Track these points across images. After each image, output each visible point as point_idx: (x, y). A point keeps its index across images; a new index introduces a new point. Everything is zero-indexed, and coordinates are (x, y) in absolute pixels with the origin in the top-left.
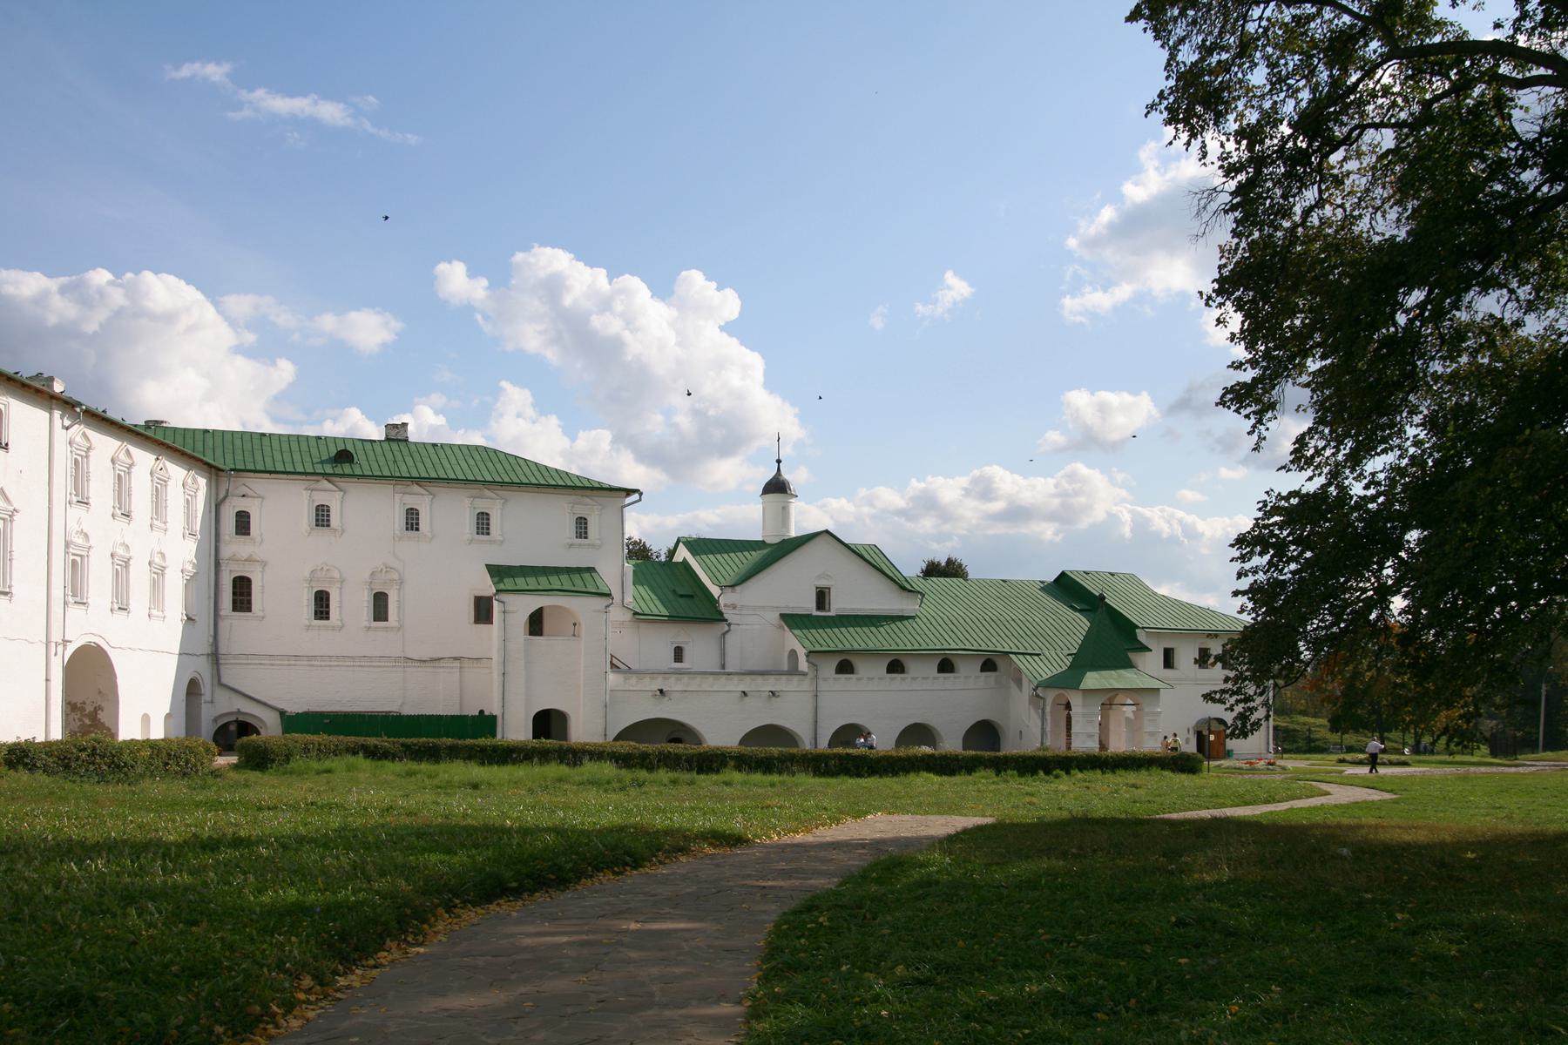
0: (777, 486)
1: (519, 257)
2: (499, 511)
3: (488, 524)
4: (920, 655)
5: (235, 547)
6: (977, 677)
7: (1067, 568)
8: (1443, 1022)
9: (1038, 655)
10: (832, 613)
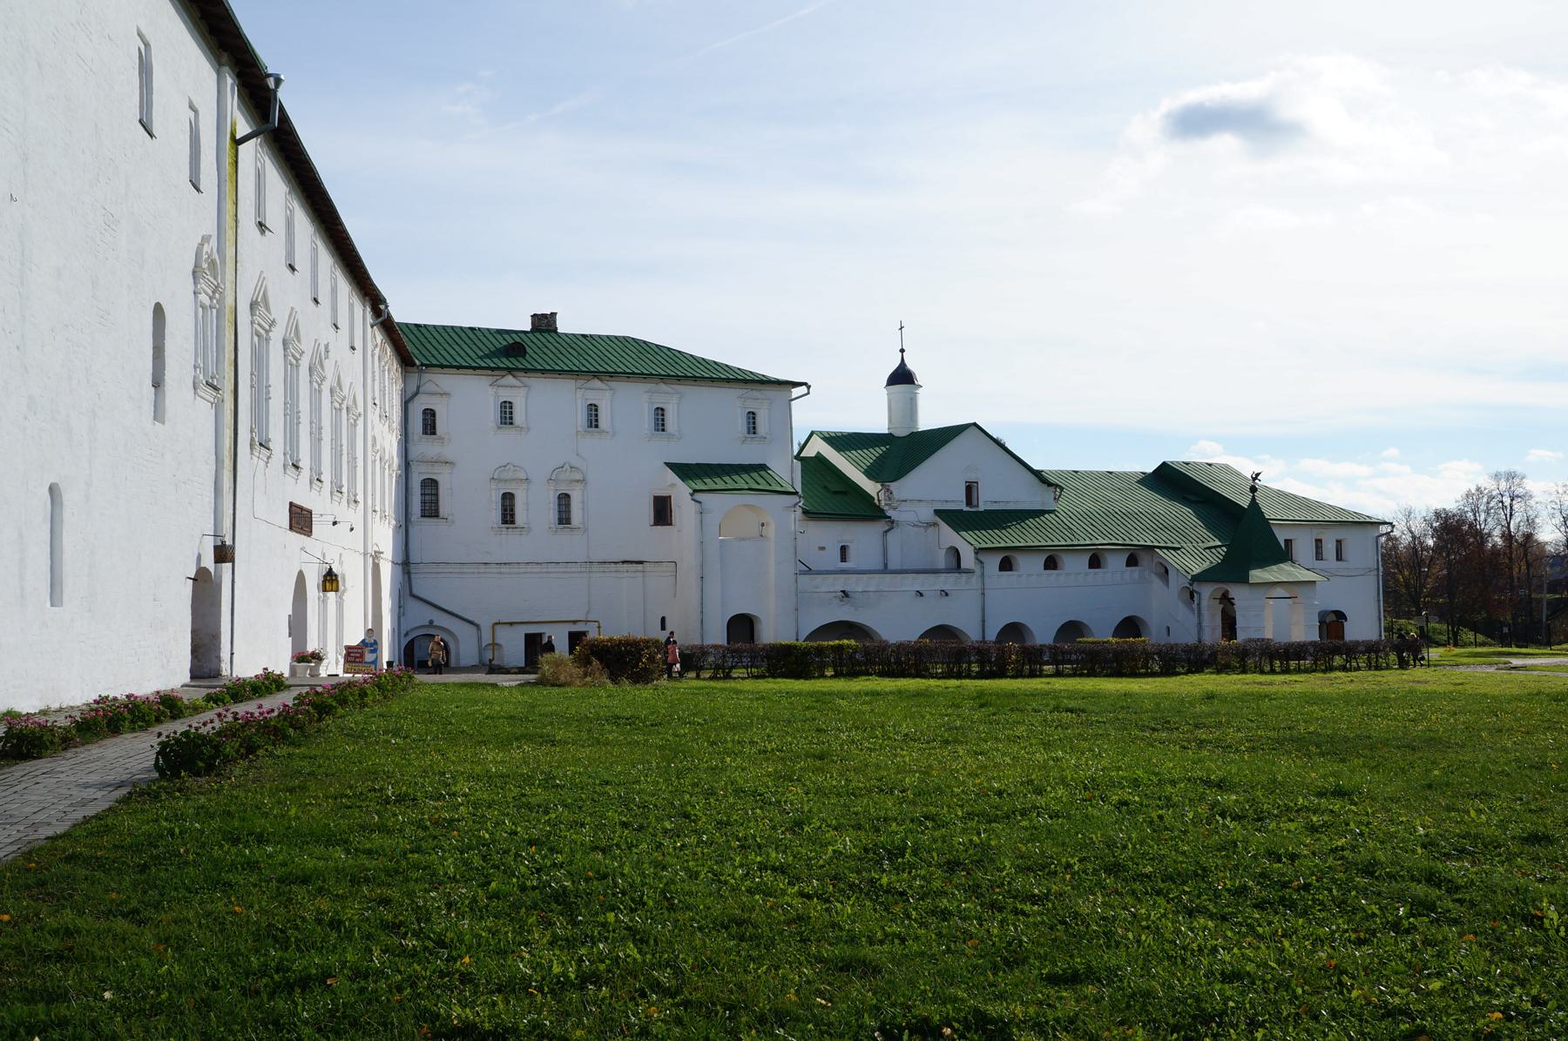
0: (902, 377)
1: (255, 129)
2: (676, 406)
3: (511, 413)
4: (1072, 549)
5: (423, 447)
6: (1087, 574)
7: (1168, 459)
8: (562, 915)
9: (1179, 549)
10: (981, 508)
